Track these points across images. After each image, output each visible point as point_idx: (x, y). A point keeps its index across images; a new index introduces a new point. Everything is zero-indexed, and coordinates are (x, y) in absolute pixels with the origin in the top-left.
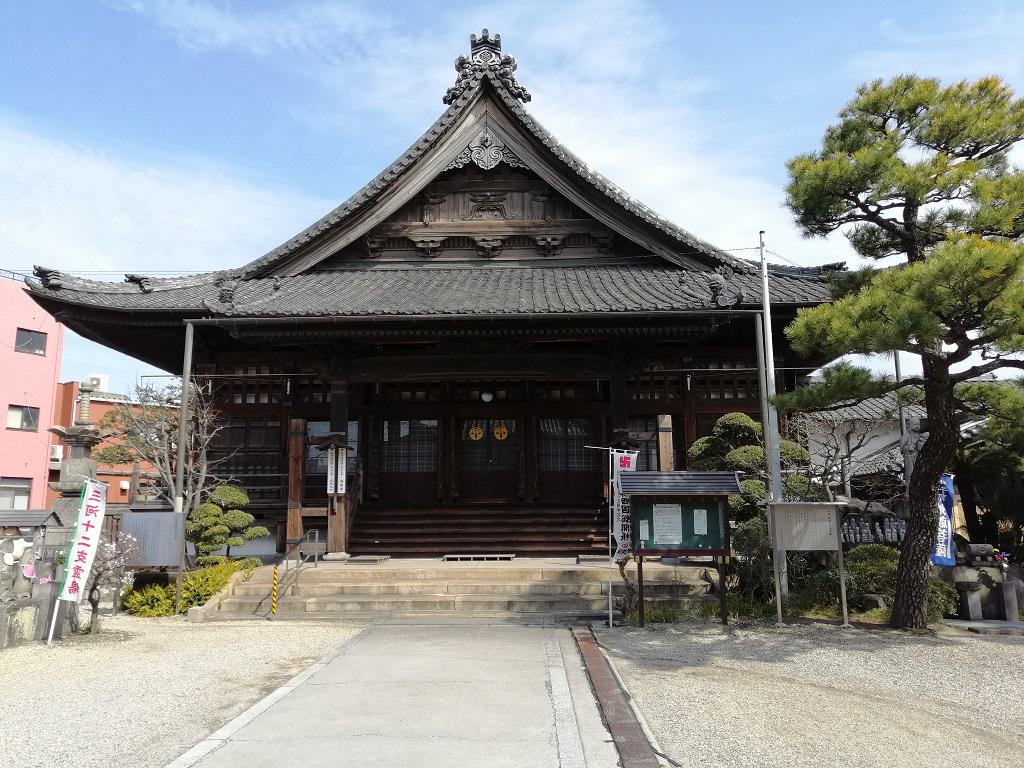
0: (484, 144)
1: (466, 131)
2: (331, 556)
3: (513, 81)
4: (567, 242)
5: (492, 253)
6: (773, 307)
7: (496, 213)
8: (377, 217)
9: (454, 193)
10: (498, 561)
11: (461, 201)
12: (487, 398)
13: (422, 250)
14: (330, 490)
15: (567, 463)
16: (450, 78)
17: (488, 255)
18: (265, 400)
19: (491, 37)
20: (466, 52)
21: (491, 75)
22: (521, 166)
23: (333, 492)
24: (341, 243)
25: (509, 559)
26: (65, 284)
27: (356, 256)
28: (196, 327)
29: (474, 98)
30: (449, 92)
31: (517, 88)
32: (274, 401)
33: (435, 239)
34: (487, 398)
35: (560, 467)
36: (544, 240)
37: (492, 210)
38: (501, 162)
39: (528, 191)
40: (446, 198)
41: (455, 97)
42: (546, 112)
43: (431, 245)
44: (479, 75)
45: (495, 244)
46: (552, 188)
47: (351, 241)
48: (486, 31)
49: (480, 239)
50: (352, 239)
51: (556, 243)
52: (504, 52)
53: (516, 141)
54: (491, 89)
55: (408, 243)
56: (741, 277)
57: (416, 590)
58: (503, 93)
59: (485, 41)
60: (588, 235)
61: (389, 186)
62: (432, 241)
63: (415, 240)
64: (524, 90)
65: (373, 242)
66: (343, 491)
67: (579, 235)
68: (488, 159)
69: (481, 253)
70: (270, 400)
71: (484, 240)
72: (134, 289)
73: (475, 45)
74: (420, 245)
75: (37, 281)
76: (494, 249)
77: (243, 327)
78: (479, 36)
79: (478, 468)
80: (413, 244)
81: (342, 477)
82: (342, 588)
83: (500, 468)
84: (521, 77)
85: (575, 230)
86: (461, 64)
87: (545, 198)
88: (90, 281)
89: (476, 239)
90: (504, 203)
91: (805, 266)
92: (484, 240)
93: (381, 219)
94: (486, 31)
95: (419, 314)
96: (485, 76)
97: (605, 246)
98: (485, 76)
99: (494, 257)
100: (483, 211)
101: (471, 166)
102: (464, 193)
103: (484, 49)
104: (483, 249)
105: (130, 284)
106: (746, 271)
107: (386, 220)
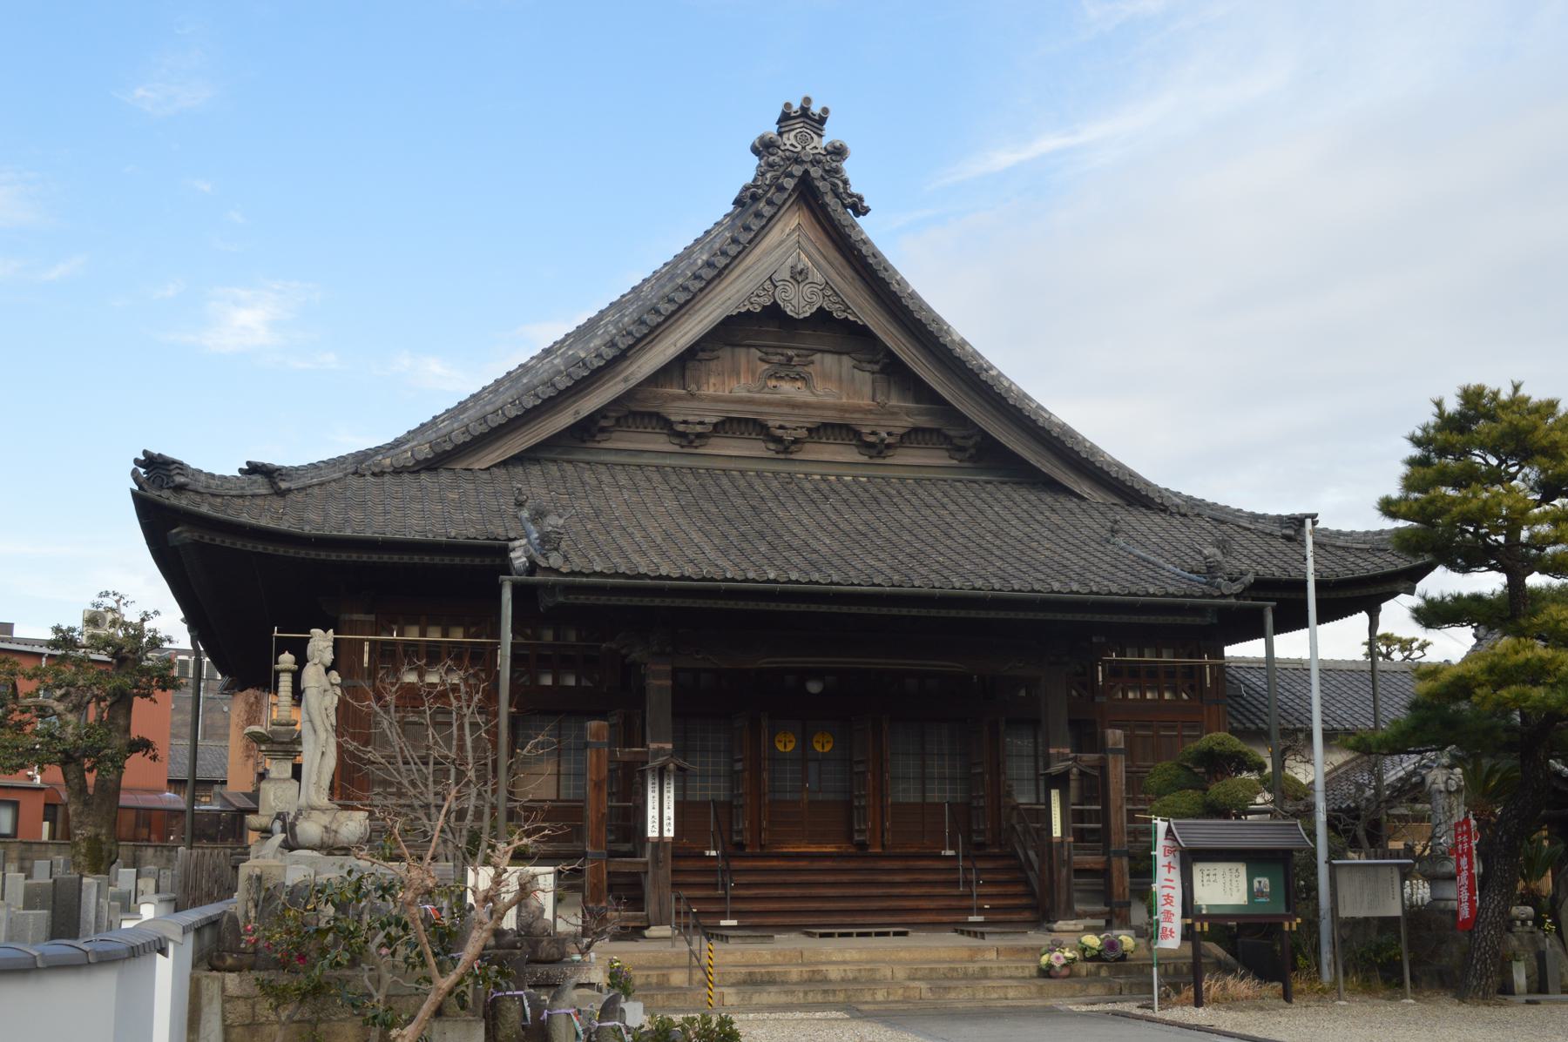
0: (798, 275)
1: (767, 253)
2: (654, 931)
3: (846, 182)
4: (913, 437)
5: (793, 448)
6: (1317, 582)
7: (799, 384)
9: (734, 345)
11: (743, 361)
13: (682, 435)
14: (652, 832)
15: (924, 792)
16: (746, 169)
17: (786, 450)
18: (571, 681)
19: (815, 109)
21: (815, 172)
22: (851, 318)
23: (656, 834)
24: (564, 419)
25: (904, 934)
29: (785, 201)
31: (851, 196)
33: (707, 420)
35: (914, 797)
36: (873, 433)
37: (794, 379)
38: (820, 309)
39: (847, 353)
40: (720, 353)
41: (755, 198)
42: (912, 240)
43: (699, 429)
44: (797, 170)
45: (802, 433)
46: (890, 354)
48: (807, 100)
49: (778, 424)
50: (584, 413)
51: (889, 440)
52: (832, 133)
53: (843, 277)
54: (802, 181)
55: (666, 424)
56: (1186, 521)
57: (851, 975)
58: (829, 199)
59: (805, 112)
60: (938, 431)
61: (651, 332)
62: (701, 423)
63: (673, 418)
64: (861, 199)
65: (605, 417)
66: (672, 834)
67: (931, 431)
68: (799, 302)
69: (772, 446)
70: (578, 680)
72: (260, 486)
74: (681, 428)
76: (796, 441)
79: (788, 797)
81: (669, 813)
82: (750, 974)
83: (820, 797)
84: (858, 175)
85: (923, 421)
86: (763, 148)
87: (876, 368)
89: (770, 424)
90: (810, 369)
92: (781, 427)
93: (633, 382)
94: (807, 100)
96: (806, 172)
97: (961, 449)
98: (806, 172)
100: (781, 378)
101: (774, 313)
102: (749, 346)
106: (1174, 510)
107: (640, 385)
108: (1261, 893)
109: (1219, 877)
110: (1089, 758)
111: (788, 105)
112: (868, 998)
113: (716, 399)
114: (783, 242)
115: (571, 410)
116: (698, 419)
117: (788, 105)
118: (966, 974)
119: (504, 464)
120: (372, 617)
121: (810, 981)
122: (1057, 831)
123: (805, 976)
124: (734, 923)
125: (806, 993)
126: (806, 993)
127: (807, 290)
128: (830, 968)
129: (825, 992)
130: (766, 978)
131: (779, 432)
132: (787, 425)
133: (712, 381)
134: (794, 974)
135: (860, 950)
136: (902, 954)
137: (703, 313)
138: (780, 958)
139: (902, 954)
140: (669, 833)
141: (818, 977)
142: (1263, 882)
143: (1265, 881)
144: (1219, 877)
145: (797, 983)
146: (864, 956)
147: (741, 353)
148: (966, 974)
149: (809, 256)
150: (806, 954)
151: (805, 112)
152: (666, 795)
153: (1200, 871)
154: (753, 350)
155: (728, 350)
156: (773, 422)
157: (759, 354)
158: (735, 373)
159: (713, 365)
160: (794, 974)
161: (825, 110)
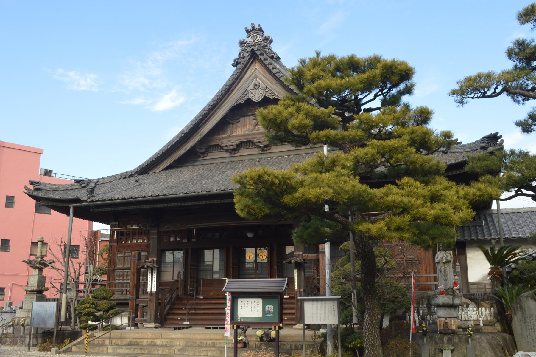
8: (200, 135)
9: (244, 116)
10: (218, 330)
12: (250, 235)
19: (257, 27)
20: (244, 36)
21: (255, 48)
22: (276, 97)
26: (43, 187)
27: (190, 158)
28: (75, 208)
30: (235, 60)
32: (178, 239)
33: (233, 144)
34: (250, 235)
38: (265, 96)
40: (240, 120)
43: (232, 147)
44: (249, 49)
47: (189, 148)
48: (252, 24)
49: (257, 141)
57: (164, 343)
59: (253, 29)
63: (222, 145)
68: (257, 96)
69: (260, 149)
71: (259, 142)
72: (77, 186)
73: (248, 32)
74: (226, 148)
75: (31, 187)
77: (97, 206)
78: (250, 28)
80: (222, 148)
81: (155, 283)
82: (131, 341)
86: (242, 43)
88: (55, 185)
91: (474, 141)
92: (259, 142)
93: (203, 135)
94: (252, 24)
95: (173, 194)
98: (253, 49)
99: (267, 151)
102: (250, 115)
103: (252, 34)
104: (259, 147)
105: (76, 184)
108: (269, 312)
109: (249, 305)
110: (312, 256)
111: (497, 133)
112: (156, 353)
113: (237, 136)
114: (251, 76)
115: (184, 148)
116: (230, 144)
117: (497, 133)
118: (206, 345)
119: (162, 170)
120: (117, 223)
121: (150, 345)
122: (296, 287)
123: (149, 343)
124: (188, 323)
125: (134, 349)
126: (134, 349)
127: (404, 137)
128: (157, 340)
129: (141, 349)
130: (136, 343)
131: (259, 144)
132: (261, 141)
133: (238, 130)
134: (145, 342)
135: (182, 334)
136: (197, 336)
137: (223, 109)
138: (154, 336)
139: (197, 336)
140: (154, 290)
141: (153, 344)
142: (270, 307)
143: (271, 307)
144: (249, 305)
145: (146, 346)
146: (28, 336)
147: (247, 118)
148: (206, 345)
149: (260, 79)
150: (163, 334)
151: (253, 29)
152: (153, 277)
153: (241, 302)
154: (251, 117)
155: (243, 118)
156: (256, 141)
157: (253, 117)
158: (245, 125)
159: (237, 124)
160: (145, 342)
161: (259, 26)
